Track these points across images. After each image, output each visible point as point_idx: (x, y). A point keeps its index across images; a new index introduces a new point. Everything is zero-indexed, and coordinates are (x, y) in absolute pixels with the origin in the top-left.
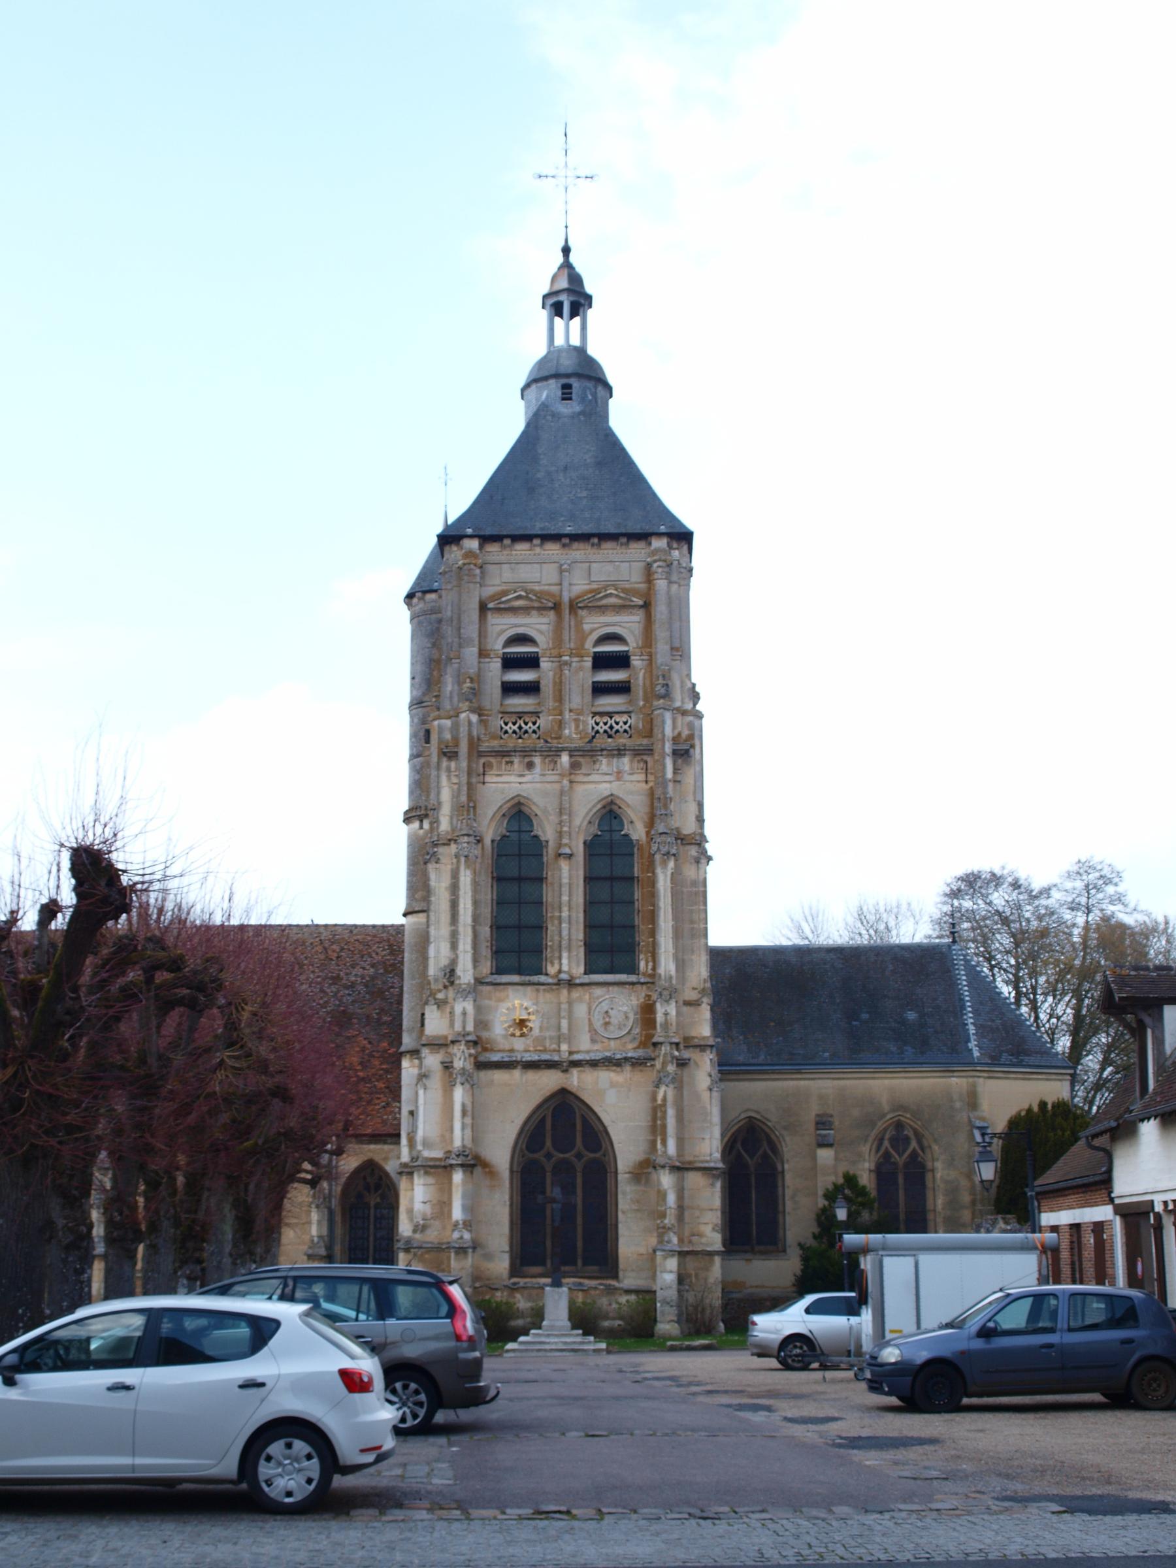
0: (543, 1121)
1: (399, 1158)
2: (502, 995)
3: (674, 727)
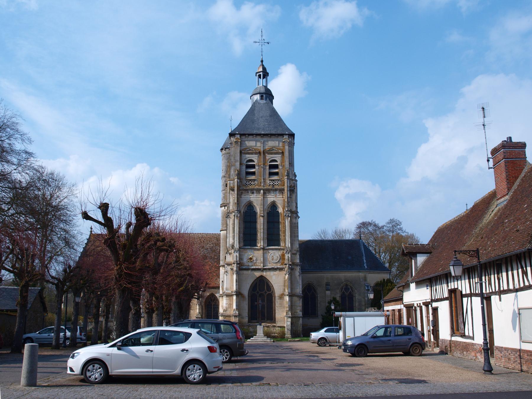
0: (256, 283)
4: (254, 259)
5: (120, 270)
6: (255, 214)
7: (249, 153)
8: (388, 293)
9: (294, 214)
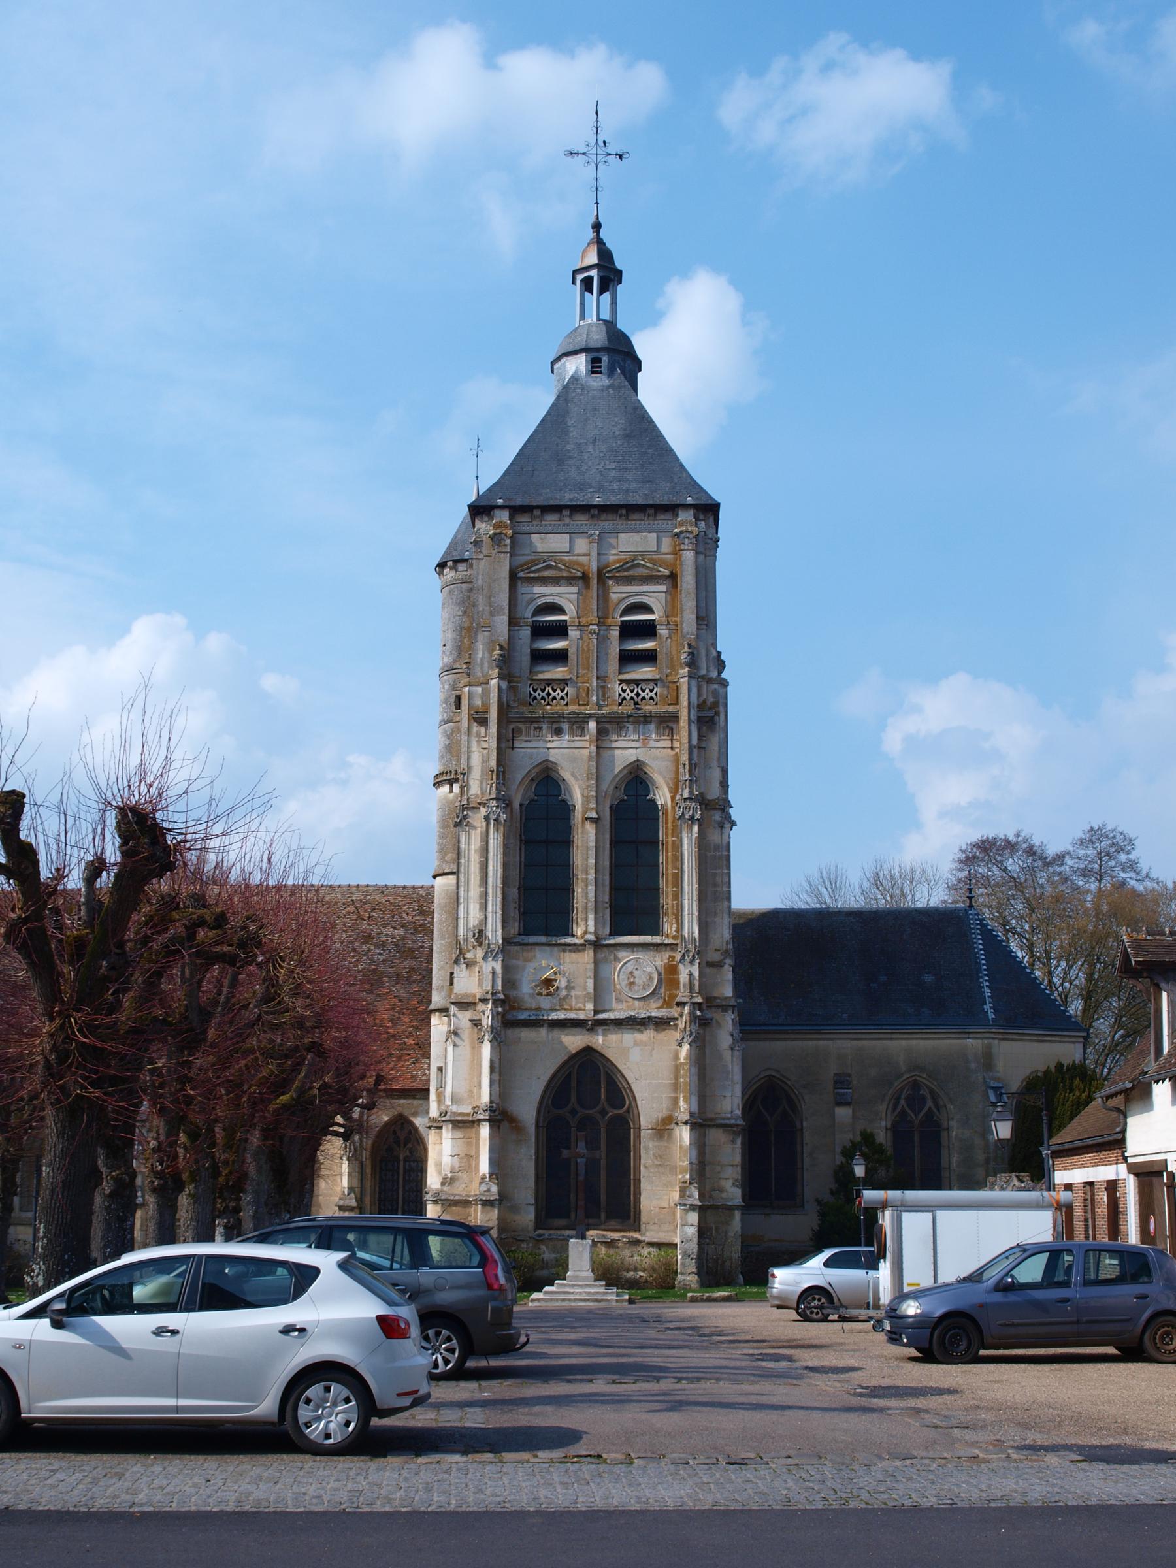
1: (428, 1113)
2: (530, 954)
3: (699, 695)
4: (562, 982)
5: (63, 1035)
6: (565, 810)
7: (544, 581)
8: (1072, 1119)
9: (714, 811)
